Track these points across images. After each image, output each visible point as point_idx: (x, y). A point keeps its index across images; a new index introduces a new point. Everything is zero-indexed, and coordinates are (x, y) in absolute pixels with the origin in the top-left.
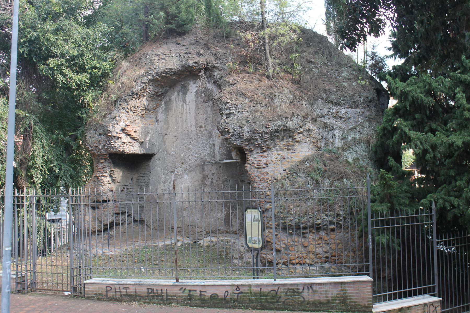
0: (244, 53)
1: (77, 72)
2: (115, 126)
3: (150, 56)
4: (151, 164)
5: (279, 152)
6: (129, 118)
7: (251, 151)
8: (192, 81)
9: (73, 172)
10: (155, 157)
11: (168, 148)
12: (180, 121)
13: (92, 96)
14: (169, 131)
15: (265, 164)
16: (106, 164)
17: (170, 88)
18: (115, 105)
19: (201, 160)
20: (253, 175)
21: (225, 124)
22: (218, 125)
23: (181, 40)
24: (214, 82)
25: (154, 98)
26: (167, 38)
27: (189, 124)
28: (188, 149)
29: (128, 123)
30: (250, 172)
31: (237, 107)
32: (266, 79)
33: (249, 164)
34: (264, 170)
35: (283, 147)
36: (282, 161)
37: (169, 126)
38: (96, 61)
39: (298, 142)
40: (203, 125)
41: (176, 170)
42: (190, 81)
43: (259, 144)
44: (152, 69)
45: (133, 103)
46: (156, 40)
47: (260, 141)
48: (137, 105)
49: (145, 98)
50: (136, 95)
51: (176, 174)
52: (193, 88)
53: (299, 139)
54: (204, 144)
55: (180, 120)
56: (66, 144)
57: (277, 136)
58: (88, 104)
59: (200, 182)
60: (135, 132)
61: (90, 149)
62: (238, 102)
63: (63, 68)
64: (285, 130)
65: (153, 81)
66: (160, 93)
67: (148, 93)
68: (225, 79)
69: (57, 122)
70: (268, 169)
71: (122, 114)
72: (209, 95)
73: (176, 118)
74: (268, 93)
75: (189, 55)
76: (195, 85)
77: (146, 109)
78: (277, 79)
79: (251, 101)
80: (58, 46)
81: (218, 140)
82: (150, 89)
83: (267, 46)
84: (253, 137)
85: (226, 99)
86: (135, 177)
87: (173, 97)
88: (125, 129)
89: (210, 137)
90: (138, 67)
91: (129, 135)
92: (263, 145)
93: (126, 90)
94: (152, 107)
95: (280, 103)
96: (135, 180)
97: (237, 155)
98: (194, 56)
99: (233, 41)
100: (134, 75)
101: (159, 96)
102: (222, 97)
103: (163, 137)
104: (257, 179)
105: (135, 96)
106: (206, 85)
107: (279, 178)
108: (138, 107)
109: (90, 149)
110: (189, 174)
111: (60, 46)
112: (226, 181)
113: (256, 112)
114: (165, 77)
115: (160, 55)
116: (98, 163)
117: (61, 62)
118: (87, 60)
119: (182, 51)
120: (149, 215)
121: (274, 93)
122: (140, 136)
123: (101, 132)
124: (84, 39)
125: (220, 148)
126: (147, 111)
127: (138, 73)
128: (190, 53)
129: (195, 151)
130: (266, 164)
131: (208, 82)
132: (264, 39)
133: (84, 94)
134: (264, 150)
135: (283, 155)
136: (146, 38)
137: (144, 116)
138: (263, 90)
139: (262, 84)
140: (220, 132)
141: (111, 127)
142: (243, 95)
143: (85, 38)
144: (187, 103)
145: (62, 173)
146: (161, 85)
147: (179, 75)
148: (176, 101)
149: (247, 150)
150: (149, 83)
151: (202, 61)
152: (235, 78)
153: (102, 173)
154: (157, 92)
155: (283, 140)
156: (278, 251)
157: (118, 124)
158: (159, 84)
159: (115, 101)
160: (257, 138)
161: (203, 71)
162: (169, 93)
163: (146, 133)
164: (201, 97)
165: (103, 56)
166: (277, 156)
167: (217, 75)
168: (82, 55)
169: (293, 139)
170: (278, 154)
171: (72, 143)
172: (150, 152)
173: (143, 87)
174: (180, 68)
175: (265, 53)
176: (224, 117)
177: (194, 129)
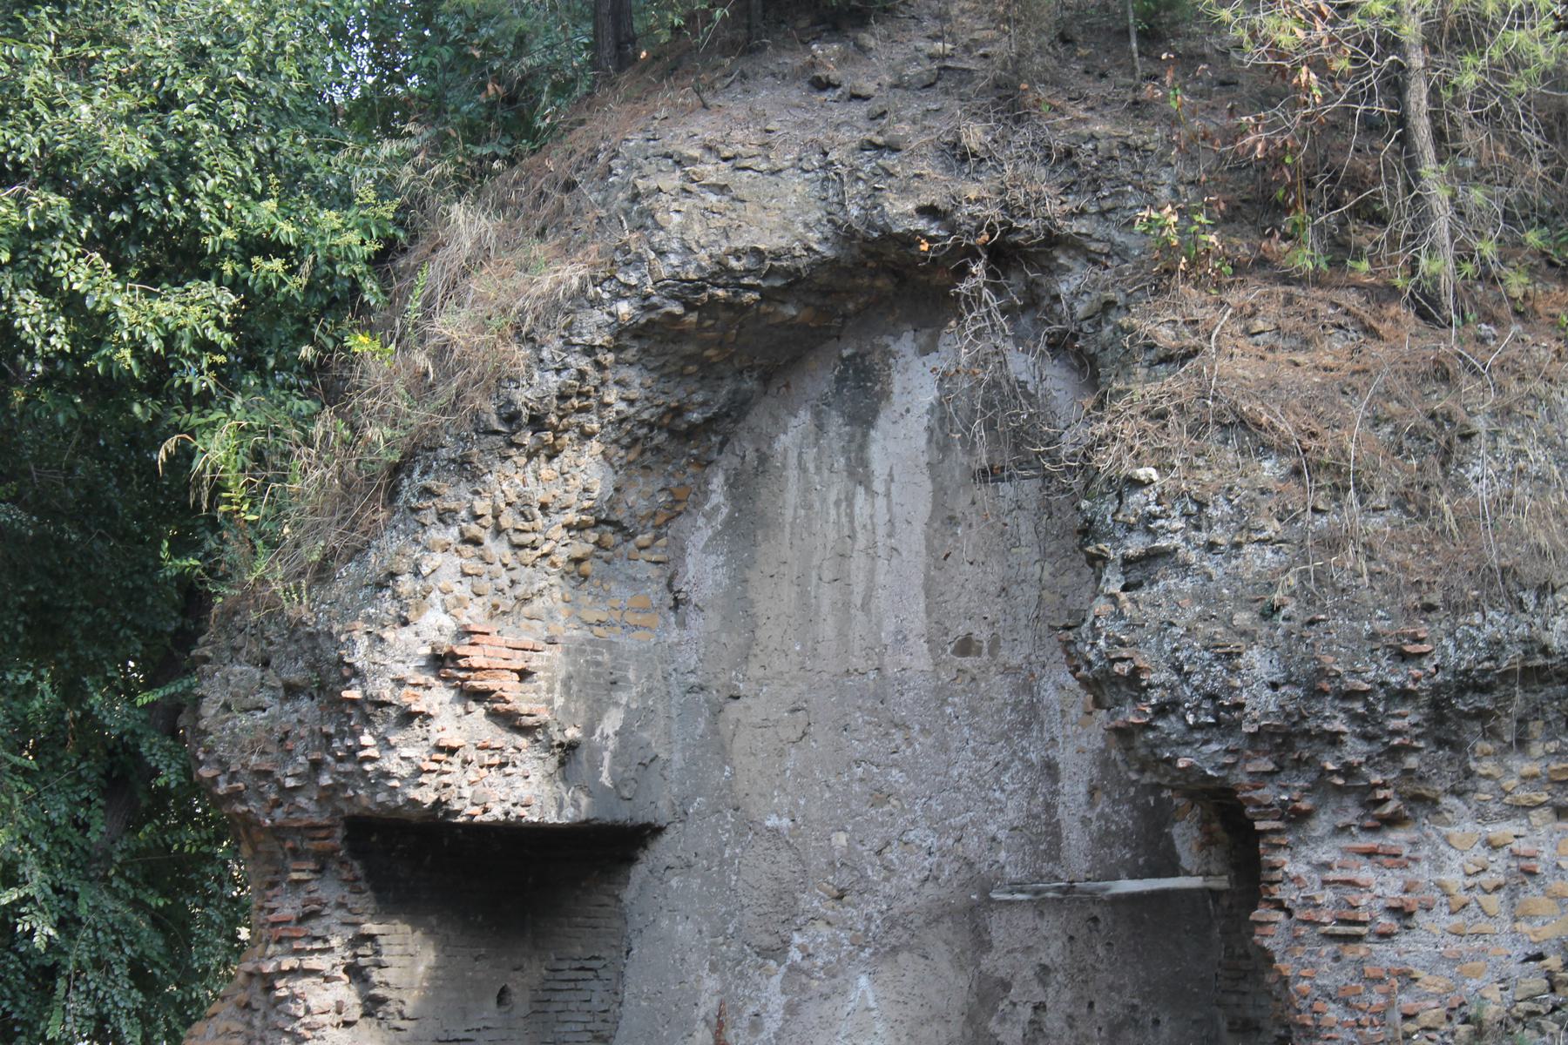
0: (1256, 142)
1: (151, 277)
2: (388, 635)
3: (629, 166)
4: (629, 895)
5: (1502, 830)
6: (485, 584)
7: (1297, 818)
8: (908, 337)
9: (154, 944)
10: (661, 852)
11: (742, 786)
13: (244, 431)
14: (755, 671)
15: (1392, 910)
16: (329, 891)
17: (766, 379)
18: (393, 494)
19: (965, 875)
20: (1304, 985)
21: (1116, 628)
22: (1068, 629)
23: (843, 60)
24: (1059, 345)
25: (658, 450)
26: (750, 49)
27: (890, 625)
28: (880, 797)
29: (474, 615)
30: (1286, 966)
31: (1197, 514)
32: (1409, 317)
33: (1279, 905)
34: (1385, 955)
35: (1522, 795)
36: (1513, 893)
37: (752, 641)
38: (271, 204)
40: (982, 634)
41: (797, 938)
42: (898, 337)
43: (1348, 771)
44: (640, 258)
45: (512, 480)
46: (675, 63)
47: (1355, 751)
48: (541, 496)
49: (595, 446)
50: (531, 429)
51: (794, 969)
52: (916, 381)
54: (987, 766)
55: (827, 596)
56: (111, 753)
57: (1481, 715)
58: (218, 488)
59: (956, 1029)
60: (524, 675)
61: (222, 789)
62: (1207, 476)
63: (58, 251)
64: (1531, 676)
65: (648, 337)
66: (695, 416)
67: (611, 415)
68: (1124, 321)
69: (23, 608)
70: (1413, 949)
71: (438, 558)
72: (1016, 432)
73: (801, 581)
74: (1416, 418)
75: (889, 160)
76: (933, 360)
77: (605, 524)
78: (1492, 319)
79: (1297, 472)
80: (30, 105)
81: (1077, 739)
82: (625, 391)
83: (1418, 97)
84: (1311, 724)
85: (1127, 459)
86: (525, 981)
88: (454, 657)
89: (1030, 715)
90: (553, 240)
91: (481, 696)
92: (1377, 779)
93: (469, 393)
94: (642, 506)
95: (1501, 486)
96: (521, 999)
97: (1208, 842)
98: (922, 166)
99: (1188, 60)
100: (517, 293)
101: (692, 432)
102: (1101, 441)
104: (1333, 1013)
105: (527, 438)
106: (1003, 364)
107: (1492, 1012)
108: (544, 507)
109: (222, 789)
110: (886, 972)
111: (39, 107)
112: (1136, 1024)
113: (1331, 544)
114: (728, 305)
115: (694, 161)
116: (272, 885)
117: (40, 214)
118: (214, 198)
119: (844, 135)
121: (1461, 415)
122: (559, 701)
123: (295, 678)
124: (195, 57)
125: (1092, 792)
126: (611, 538)
127: (547, 283)
128: (893, 148)
129: (927, 808)
130: (1401, 913)
131: (1018, 340)
132: (1392, 43)
133: (195, 420)
134: (1388, 809)
135: (1522, 846)
136: (619, 46)
137: (586, 567)
138: (1388, 395)
139: (1378, 350)
140: (1084, 683)
141: (363, 643)
142: (1239, 426)
143: (203, 52)
144: (878, 486)
145: (81, 951)
146: (706, 366)
147: (827, 292)
148: (802, 468)
149: (1265, 809)
150: (618, 349)
151: (976, 197)
152: (1198, 314)
153: (297, 952)
154: (678, 412)
155: (1522, 743)
157: (405, 623)
158: (689, 359)
159: (396, 469)
160: (1338, 725)
161: (978, 268)
162: (758, 417)
163: (596, 683)
164: (970, 447)
165: (328, 168)
166: (1482, 854)
167: (1076, 295)
168: (183, 165)
170: (1492, 845)
171: (153, 749)
172: (622, 814)
173: (582, 375)
174: (827, 251)
175: (1404, 140)
176: (1113, 582)
177: (919, 659)
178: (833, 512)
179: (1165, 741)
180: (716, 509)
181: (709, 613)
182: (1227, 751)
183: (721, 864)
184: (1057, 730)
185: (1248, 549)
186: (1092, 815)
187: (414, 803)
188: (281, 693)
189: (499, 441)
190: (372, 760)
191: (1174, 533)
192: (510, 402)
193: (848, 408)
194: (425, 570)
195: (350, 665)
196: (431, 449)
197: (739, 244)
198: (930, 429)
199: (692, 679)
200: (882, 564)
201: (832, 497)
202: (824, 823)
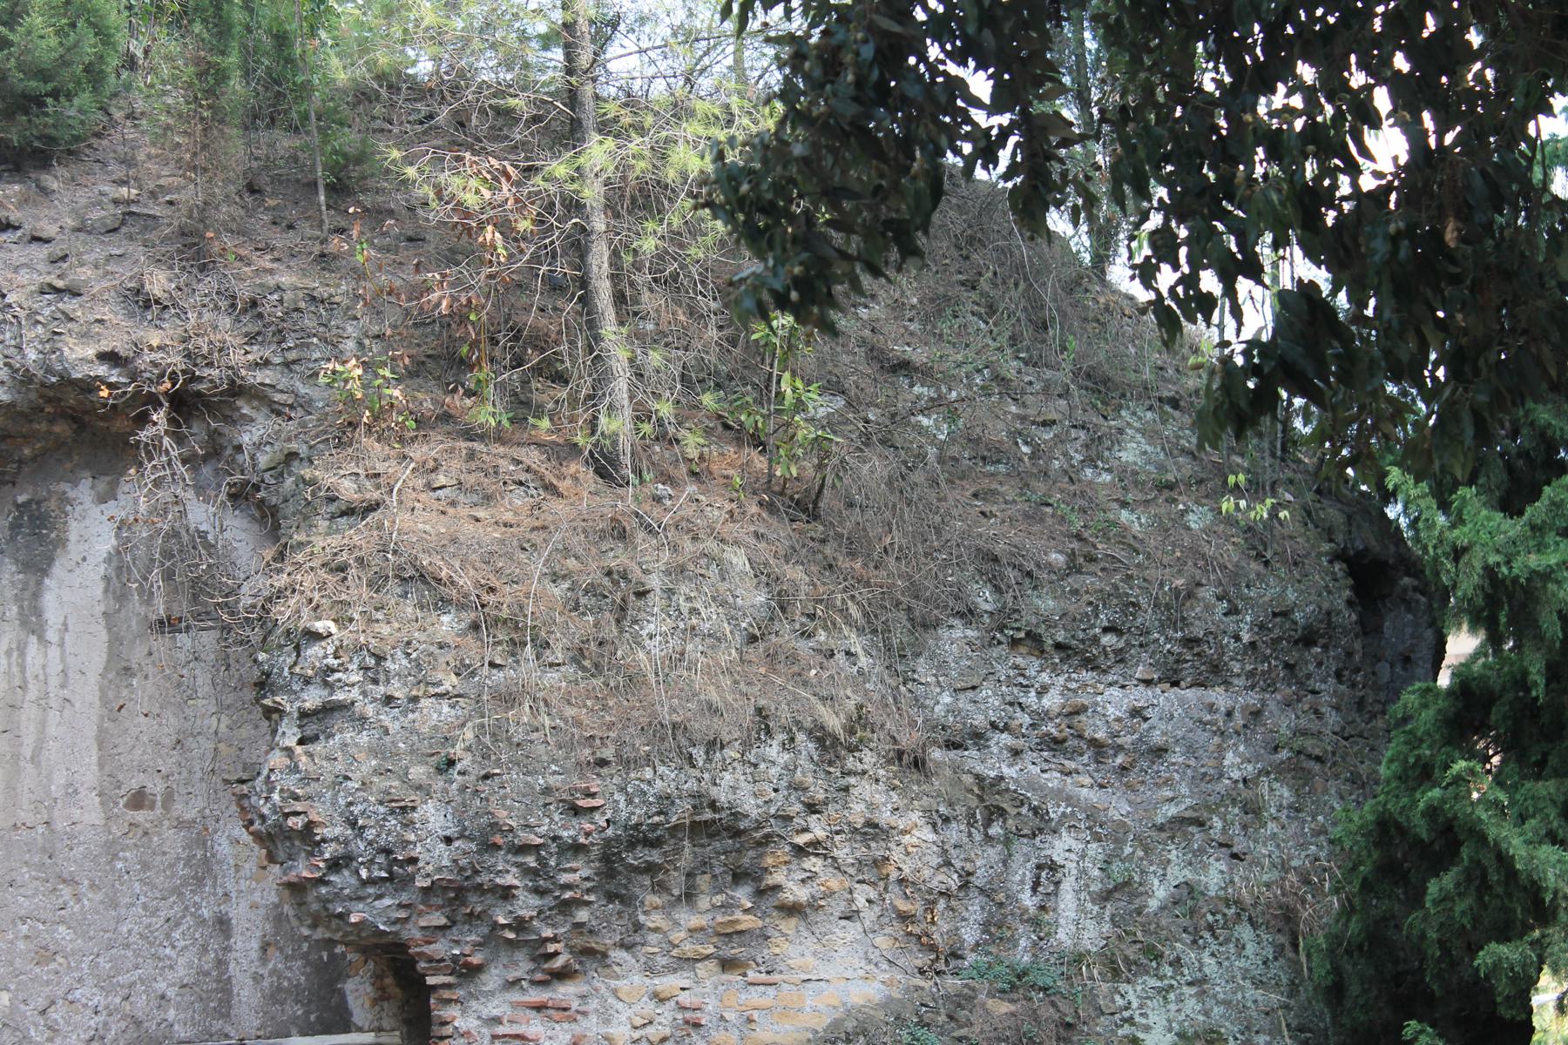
27: (60, 779)
35: (688, 948)
39: (792, 910)
42: (76, 484)
53: (801, 894)
54: (158, 922)
144: (52, 635)
155: (689, 896)
169: (760, 893)
177: (90, 812)
182: (400, 906)
185: (424, 703)
186: (264, 971)
191: (351, 686)
193: (22, 555)
198: (106, 578)
200: (53, 716)
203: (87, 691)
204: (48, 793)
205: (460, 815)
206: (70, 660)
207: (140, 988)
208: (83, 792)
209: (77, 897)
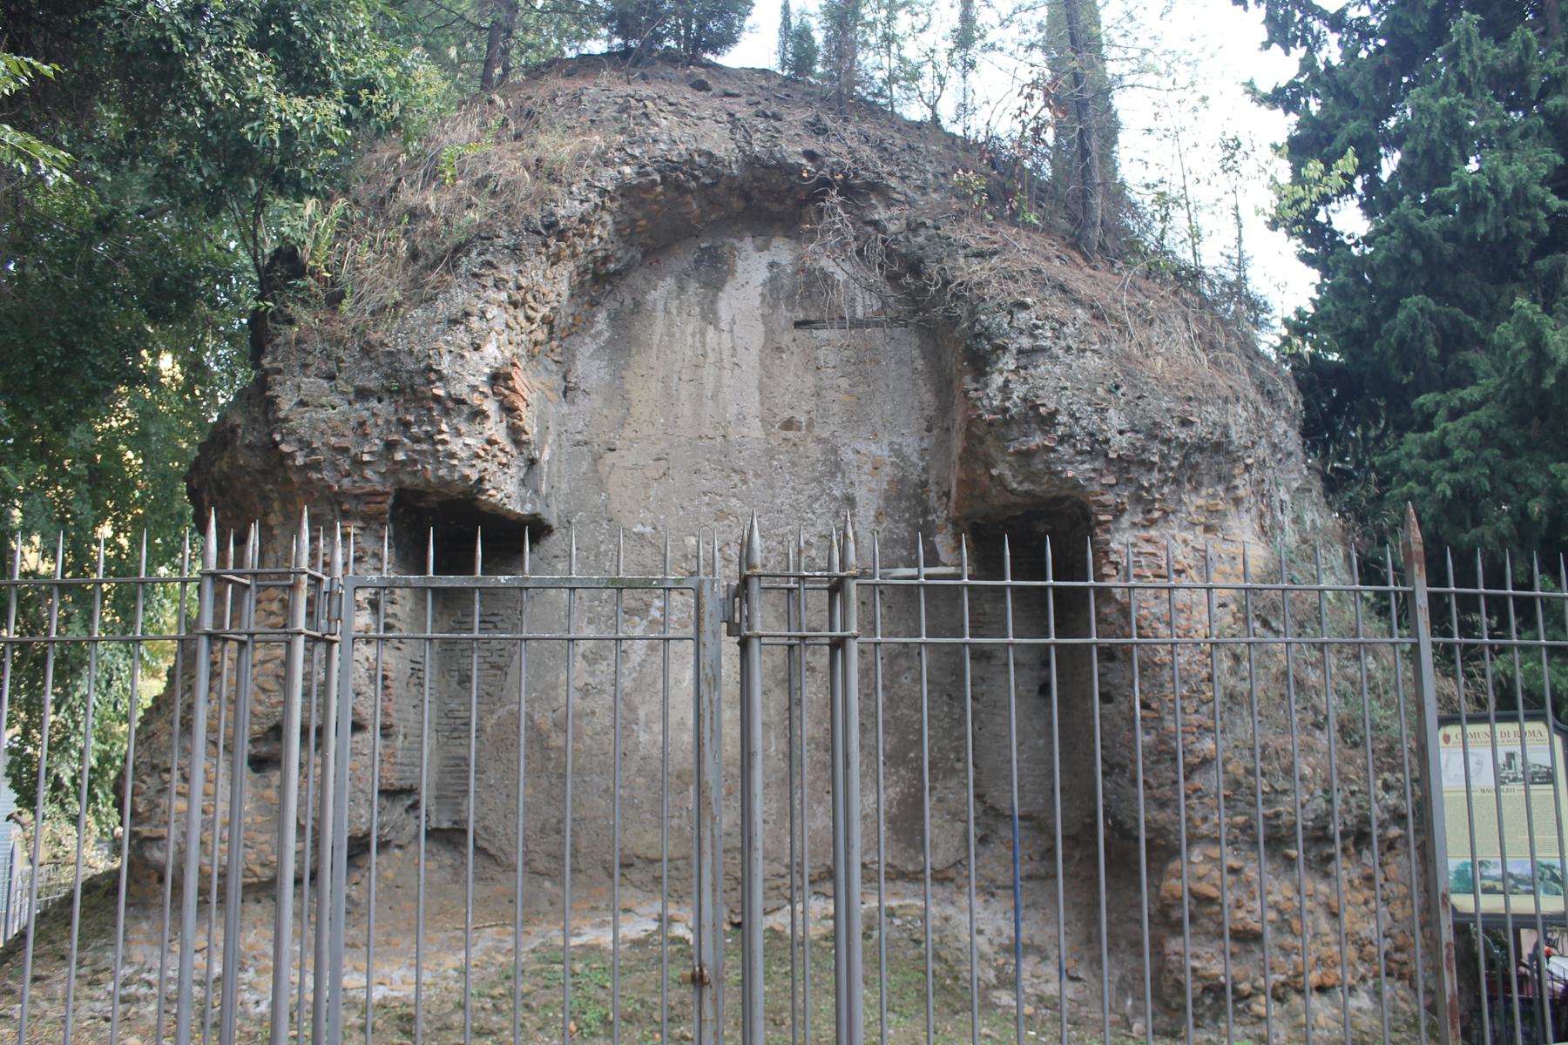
2: (466, 354)
7: (1119, 512)
11: (615, 505)
12: (684, 395)
14: (628, 433)
27: (733, 410)
28: (721, 515)
42: (741, 240)
52: (755, 266)
54: (802, 498)
55: (686, 390)
61: (300, 461)
66: (612, 266)
73: (665, 381)
76: (766, 257)
87: (653, 295)
103: (597, 458)
120: (505, 807)
144: (724, 325)
148: (667, 311)
156: (1247, 938)
162: (636, 279)
169: (1227, 490)
177: (755, 430)
178: (690, 340)
179: (1060, 460)
180: (600, 333)
181: (594, 396)
182: (1094, 470)
183: (596, 556)
184: (854, 477)
185: (1088, 354)
186: (880, 529)
187: (466, 478)
188: (352, 397)
189: (539, 240)
190: (444, 442)
191: (1046, 338)
192: (552, 214)
193: (703, 278)
194: (489, 316)
195: (437, 372)
196: (488, 239)
197: (704, 147)
198: (762, 295)
199: (579, 437)
200: (727, 373)
201: (690, 329)
202: (678, 530)
203: (751, 360)
204: (725, 419)
205: (1130, 417)
206: (738, 341)
207: (791, 537)
208: (749, 418)
209: (745, 482)
